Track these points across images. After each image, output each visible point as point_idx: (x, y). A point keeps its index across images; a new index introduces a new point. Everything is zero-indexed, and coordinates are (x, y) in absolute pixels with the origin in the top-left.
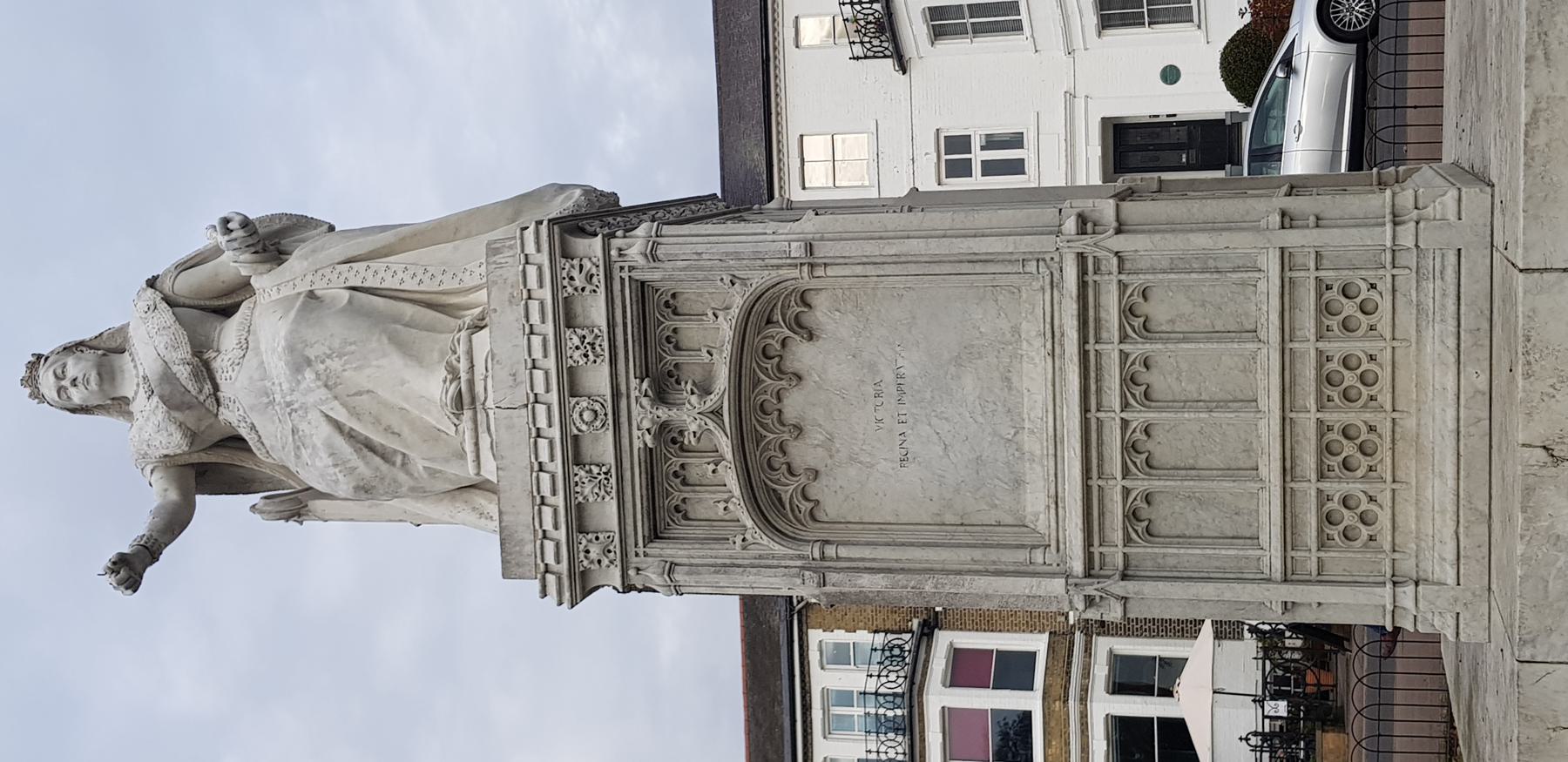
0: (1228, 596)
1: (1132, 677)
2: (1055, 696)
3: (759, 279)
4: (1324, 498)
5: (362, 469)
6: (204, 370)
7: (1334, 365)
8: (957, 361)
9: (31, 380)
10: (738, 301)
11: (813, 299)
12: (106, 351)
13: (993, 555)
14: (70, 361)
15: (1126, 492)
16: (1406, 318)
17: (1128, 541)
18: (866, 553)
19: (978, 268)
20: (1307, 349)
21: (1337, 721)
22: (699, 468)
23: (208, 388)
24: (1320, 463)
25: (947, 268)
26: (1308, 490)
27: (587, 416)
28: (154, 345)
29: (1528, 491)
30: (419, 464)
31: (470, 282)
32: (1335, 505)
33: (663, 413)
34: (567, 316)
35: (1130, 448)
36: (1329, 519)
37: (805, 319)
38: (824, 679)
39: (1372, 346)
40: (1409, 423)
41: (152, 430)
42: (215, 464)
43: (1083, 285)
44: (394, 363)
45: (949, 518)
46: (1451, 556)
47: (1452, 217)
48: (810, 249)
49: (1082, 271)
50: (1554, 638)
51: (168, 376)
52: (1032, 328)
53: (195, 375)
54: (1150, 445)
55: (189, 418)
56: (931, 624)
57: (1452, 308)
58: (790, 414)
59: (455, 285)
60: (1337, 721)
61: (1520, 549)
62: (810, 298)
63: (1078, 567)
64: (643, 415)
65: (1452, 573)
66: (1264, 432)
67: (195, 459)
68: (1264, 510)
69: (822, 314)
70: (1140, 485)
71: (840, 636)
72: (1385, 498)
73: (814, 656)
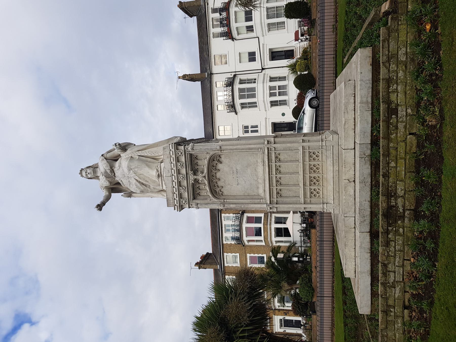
0: (294, 207)
1: (278, 221)
2: (265, 224)
3: (212, 153)
4: (310, 189)
5: (142, 188)
6: (112, 171)
7: (312, 166)
8: (247, 167)
9: (81, 173)
10: (208, 157)
11: (221, 156)
12: (95, 168)
13: (254, 200)
14: (88, 170)
15: (277, 189)
16: (324, 157)
17: (277, 197)
18: (232, 201)
19: (250, 150)
20: (307, 163)
21: (314, 227)
22: (202, 187)
23: (113, 174)
24: (310, 183)
25: (245, 150)
26: (308, 188)
27: (182, 178)
28: (103, 167)
29: (345, 187)
30: (152, 187)
31: (160, 154)
32: (312, 190)
33: (195, 177)
34: (178, 160)
35: (277, 181)
36: (312, 193)
37: (220, 160)
38: (224, 223)
39: (318, 163)
40: (325, 176)
41: (103, 182)
42: (115, 187)
43: (268, 153)
44: (147, 169)
45: (246, 194)
46: (333, 199)
47: (332, 140)
48: (221, 147)
49: (268, 151)
50: (350, 213)
51: (106, 172)
52: (260, 161)
53: (111, 172)
54: (281, 181)
55: (110, 179)
56: (243, 212)
57: (332, 155)
58: (218, 177)
59: (157, 155)
60: (314, 227)
61: (344, 197)
62: (221, 156)
63: (268, 202)
64: (192, 178)
65: (333, 202)
66: (300, 178)
67: (111, 187)
68: (300, 191)
69: (223, 159)
70: (279, 188)
71: (227, 215)
72: (321, 189)
73: (223, 219)
